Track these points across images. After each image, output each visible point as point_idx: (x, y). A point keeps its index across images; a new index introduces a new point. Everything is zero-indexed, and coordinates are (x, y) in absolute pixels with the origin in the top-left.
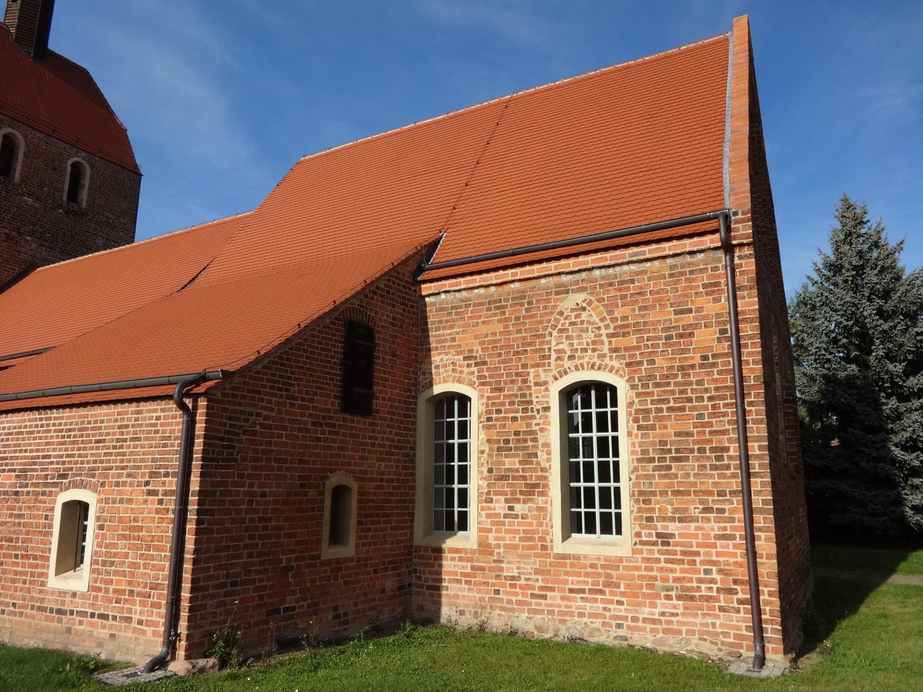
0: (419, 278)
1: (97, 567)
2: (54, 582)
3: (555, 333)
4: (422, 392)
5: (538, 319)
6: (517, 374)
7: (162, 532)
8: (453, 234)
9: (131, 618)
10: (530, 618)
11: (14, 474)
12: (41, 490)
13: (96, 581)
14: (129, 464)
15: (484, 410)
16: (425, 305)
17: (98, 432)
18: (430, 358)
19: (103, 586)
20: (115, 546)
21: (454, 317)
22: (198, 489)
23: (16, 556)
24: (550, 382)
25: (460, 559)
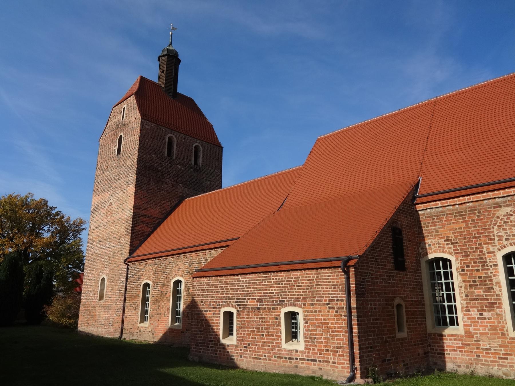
0: (415, 202)
1: (307, 340)
2: (285, 346)
3: (496, 227)
4: (422, 258)
5: (485, 220)
6: (476, 248)
7: (340, 324)
8: (425, 178)
9: (329, 361)
10: (499, 369)
11: (255, 300)
12: (271, 307)
13: (307, 345)
14: (317, 296)
15: (459, 266)
16: (419, 215)
17: (297, 282)
18: (425, 241)
19: (311, 348)
20: (315, 331)
21: (436, 220)
22: (356, 306)
23: (263, 335)
24: (496, 252)
25: (455, 340)
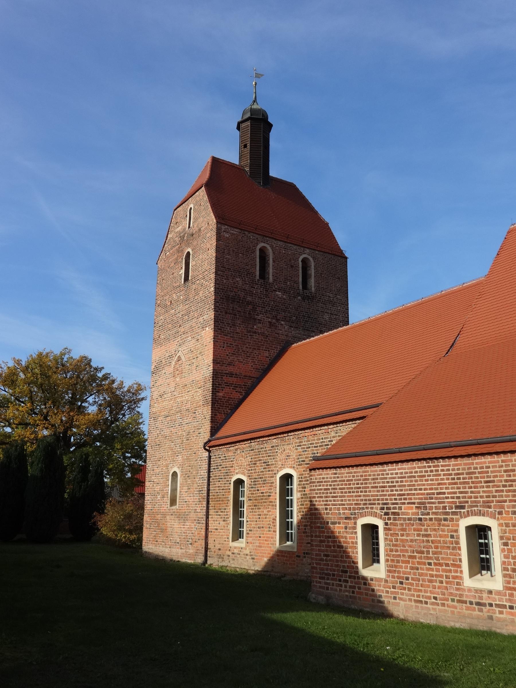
2: (468, 582)
11: (414, 506)
13: (509, 582)
